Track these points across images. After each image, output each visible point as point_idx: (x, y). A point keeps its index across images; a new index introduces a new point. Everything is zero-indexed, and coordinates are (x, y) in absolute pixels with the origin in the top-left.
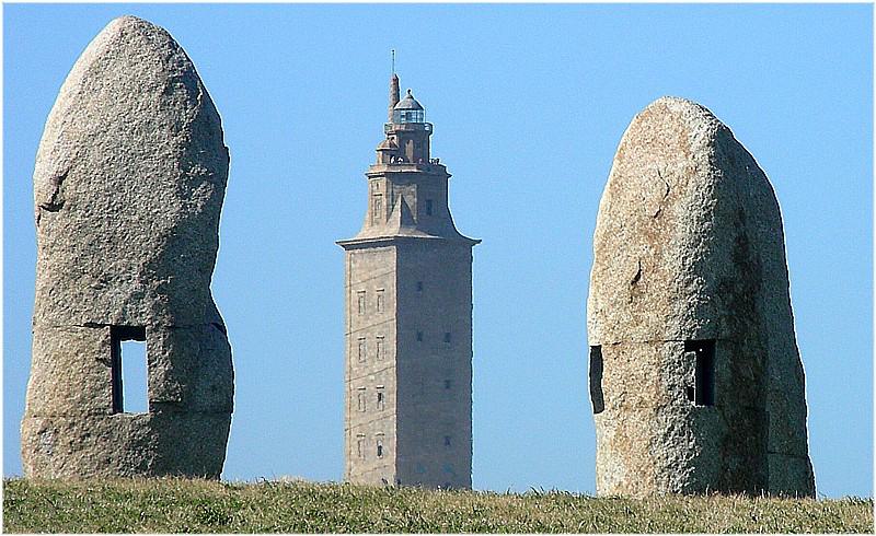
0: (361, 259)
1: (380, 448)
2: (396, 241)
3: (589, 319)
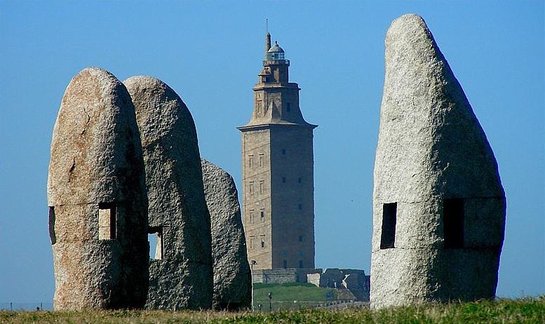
0: (251, 136)
1: (263, 243)
2: (270, 126)
3: (48, 192)
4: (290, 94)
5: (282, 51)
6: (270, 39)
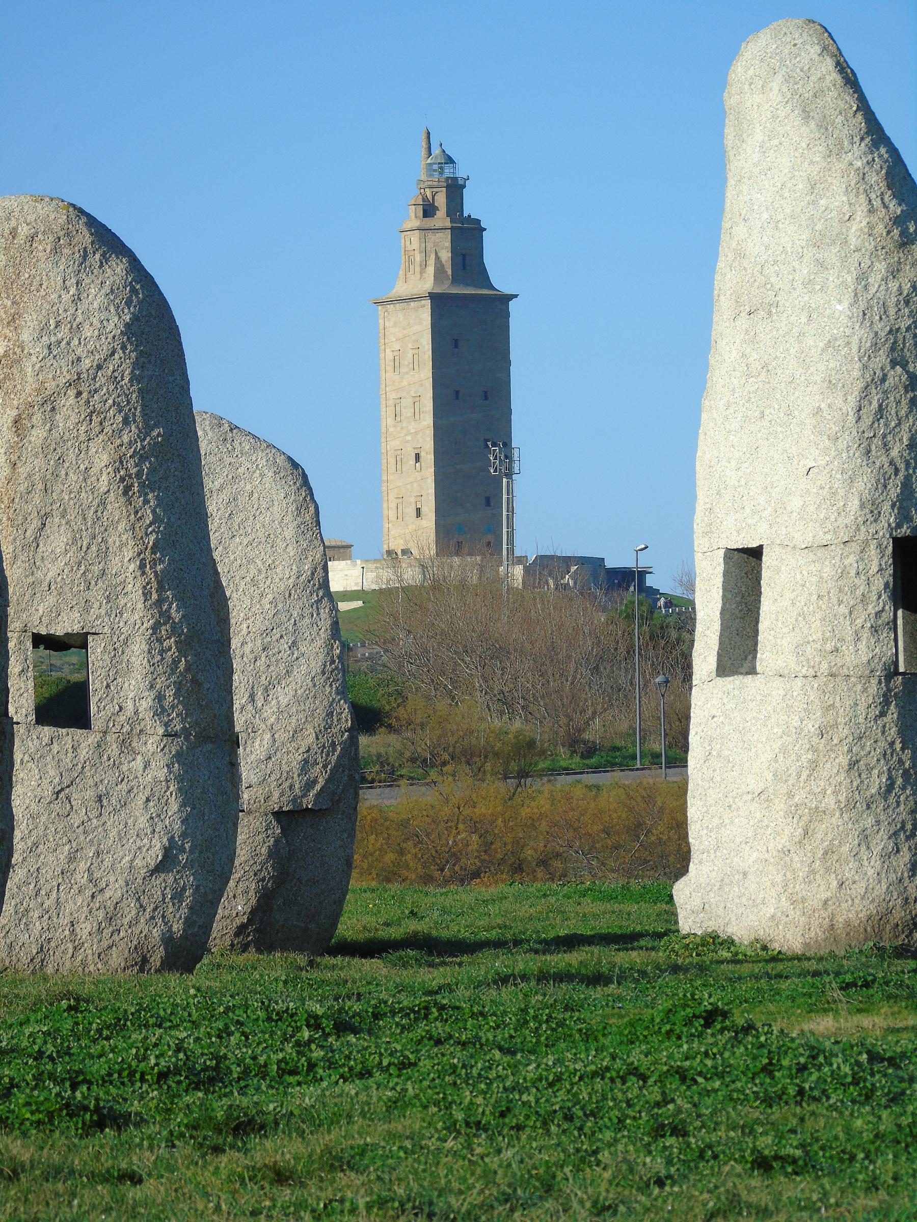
4: (467, 238)
5: (450, 160)
6: (429, 138)
